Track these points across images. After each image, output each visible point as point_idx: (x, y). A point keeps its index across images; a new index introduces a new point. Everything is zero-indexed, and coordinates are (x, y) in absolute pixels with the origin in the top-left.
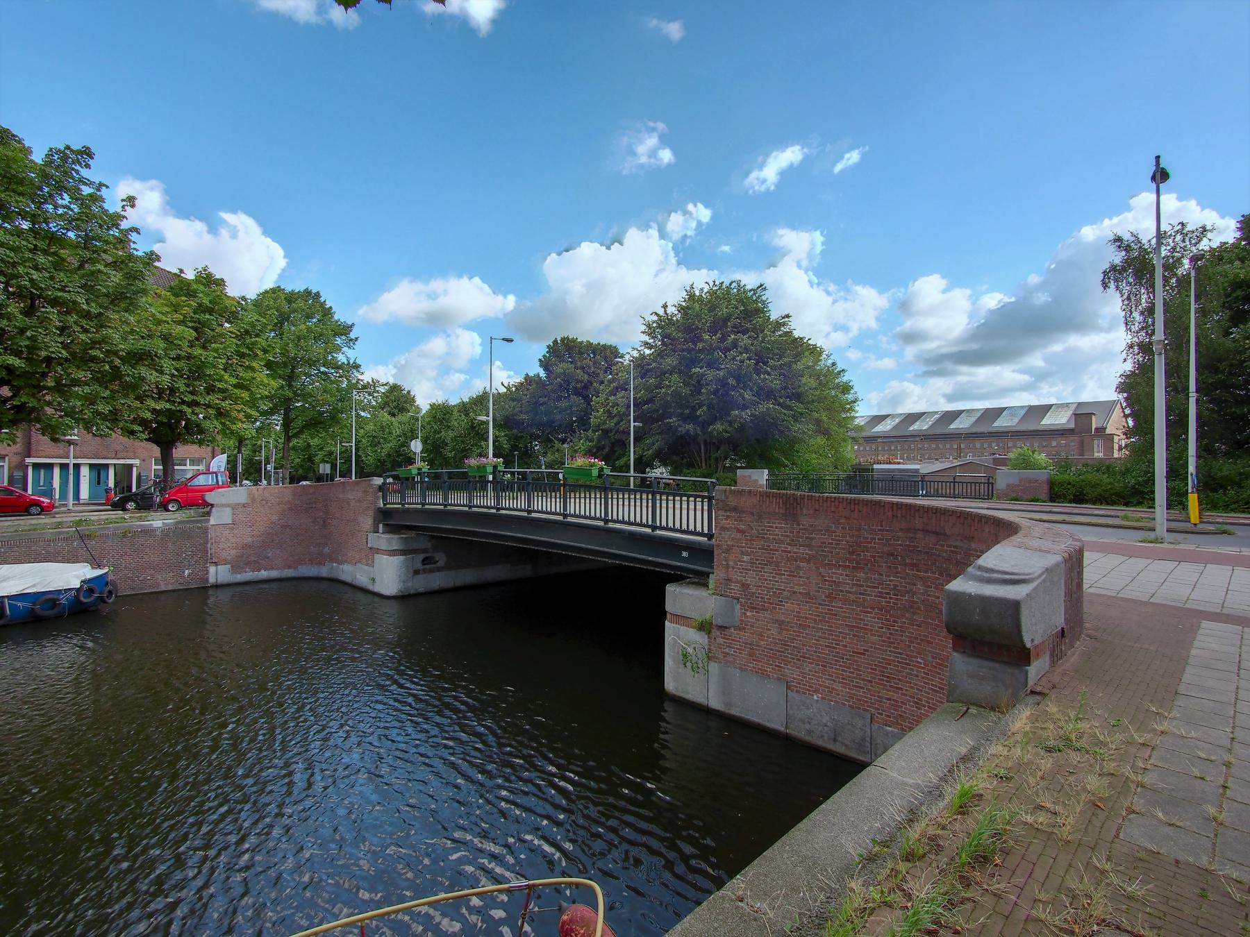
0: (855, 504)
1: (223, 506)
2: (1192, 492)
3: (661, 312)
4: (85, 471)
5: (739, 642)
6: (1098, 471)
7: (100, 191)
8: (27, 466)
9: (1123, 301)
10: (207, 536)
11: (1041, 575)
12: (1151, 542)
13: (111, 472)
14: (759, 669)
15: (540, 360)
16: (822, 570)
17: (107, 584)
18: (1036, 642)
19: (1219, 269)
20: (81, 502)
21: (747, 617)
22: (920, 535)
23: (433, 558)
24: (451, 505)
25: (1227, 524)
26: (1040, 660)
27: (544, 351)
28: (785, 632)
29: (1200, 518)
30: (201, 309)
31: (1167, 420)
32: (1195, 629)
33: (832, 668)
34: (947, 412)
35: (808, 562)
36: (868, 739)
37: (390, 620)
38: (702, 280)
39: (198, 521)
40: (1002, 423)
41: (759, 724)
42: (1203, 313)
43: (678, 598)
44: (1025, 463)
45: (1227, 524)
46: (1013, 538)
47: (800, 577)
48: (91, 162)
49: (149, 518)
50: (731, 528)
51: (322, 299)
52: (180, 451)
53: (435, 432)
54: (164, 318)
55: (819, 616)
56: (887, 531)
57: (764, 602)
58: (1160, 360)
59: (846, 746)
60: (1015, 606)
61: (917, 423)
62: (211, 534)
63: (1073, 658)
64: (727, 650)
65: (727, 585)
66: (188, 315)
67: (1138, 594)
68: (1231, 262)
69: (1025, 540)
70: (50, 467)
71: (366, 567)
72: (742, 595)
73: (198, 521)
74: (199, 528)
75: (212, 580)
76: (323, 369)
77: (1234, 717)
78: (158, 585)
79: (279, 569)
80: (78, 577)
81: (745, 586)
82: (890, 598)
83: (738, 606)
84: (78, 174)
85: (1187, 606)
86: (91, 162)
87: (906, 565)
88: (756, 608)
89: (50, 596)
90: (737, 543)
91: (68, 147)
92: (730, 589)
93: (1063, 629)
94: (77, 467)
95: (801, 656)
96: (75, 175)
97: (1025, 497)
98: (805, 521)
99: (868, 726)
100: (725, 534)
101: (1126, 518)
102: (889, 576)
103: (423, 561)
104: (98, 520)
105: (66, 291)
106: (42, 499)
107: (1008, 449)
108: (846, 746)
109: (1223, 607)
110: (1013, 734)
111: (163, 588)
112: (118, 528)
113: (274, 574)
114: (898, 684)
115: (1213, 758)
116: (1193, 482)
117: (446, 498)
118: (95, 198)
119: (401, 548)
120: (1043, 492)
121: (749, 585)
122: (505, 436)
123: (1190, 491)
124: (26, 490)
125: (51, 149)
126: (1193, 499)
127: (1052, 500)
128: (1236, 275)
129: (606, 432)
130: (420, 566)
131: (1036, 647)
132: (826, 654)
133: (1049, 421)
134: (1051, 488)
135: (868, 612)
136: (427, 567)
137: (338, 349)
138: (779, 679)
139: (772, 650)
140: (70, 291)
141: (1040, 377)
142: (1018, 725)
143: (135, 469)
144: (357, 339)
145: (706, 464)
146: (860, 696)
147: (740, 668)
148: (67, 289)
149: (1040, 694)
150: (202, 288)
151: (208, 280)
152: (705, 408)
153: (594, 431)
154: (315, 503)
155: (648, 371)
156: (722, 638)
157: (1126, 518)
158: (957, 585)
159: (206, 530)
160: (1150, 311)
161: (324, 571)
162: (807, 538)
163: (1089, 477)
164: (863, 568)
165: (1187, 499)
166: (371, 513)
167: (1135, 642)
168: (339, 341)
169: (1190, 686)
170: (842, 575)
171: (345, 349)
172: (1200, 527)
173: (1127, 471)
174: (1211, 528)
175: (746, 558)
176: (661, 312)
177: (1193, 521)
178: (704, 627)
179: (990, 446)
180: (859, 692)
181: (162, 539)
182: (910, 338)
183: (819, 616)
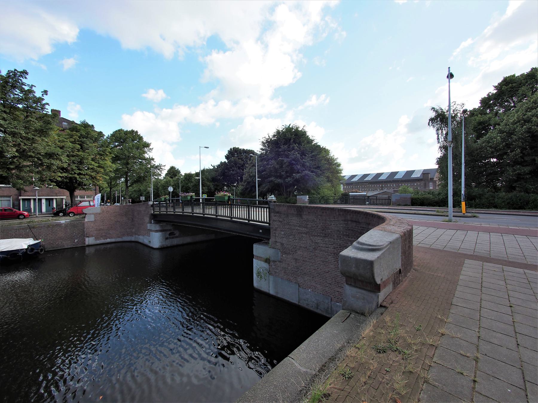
0: (324, 210)
1: (90, 214)
2: (463, 201)
4: (44, 201)
5: (280, 267)
6: (429, 194)
7: (32, 88)
8: (20, 200)
10: (84, 226)
11: (387, 246)
12: (447, 221)
13: (55, 201)
14: (288, 278)
15: (225, 156)
16: (311, 237)
17: (40, 247)
18: (384, 280)
19: (473, 118)
21: (283, 257)
22: (349, 222)
23: (173, 233)
24: (186, 213)
25: (475, 213)
26: (386, 288)
28: (297, 263)
29: (466, 211)
30: (81, 136)
31: (453, 174)
32: (462, 264)
33: (316, 278)
35: (306, 234)
36: (330, 308)
37: (157, 258)
39: (80, 220)
41: (288, 301)
42: (467, 134)
43: (258, 249)
44: (405, 191)
45: (475, 213)
46: (381, 226)
47: (303, 240)
48: (27, 76)
49: (60, 219)
51: (139, 134)
52: (77, 192)
53: (186, 184)
54: (66, 140)
55: (310, 257)
56: (337, 221)
57: (290, 251)
58: (450, 150)
59: (322, 311)
60: (371, 263)
62: (86, 225)
63: (405, 284)
64: (276, 271)
65: (275, 244)
66: (76, 139)
67: (439, 246)
68: (477, 115)
69: (386, 226)
71: (147, 237)
73: (80, 220)
74: (80, 223)
75: (87, 243)
76: (140, 160)
77: (480, 320)
79: (114, 238)
80: (26, 244)
81: (282, 244)
82: (338, 249)
83: (280, 253)
84: (21, 81)
85: (459, 252)
86: (27, 76)
87: (344, 235)
89: (14, 252)
91: (15, 70)
92: (277, 245)
93: (400, 269)
94: (40, 200)
95: (304, 273)
96: (20, 81)
97: (402, 204)
98: (305, 217)
99: (330, 303)
101: (438, 212)
102: (338, 240)
103: (169, 234)
104: (38, 221)
105: (16, 129)
106: (24, 213)
107: (399, 187)
108: (322, 311)
109: (474, 252)
110: (363, 338)
111: (66, 247)
112: (46, 224)
113: (113, 240)
114: (341, 285)
115: (468, 355)
116: (463, 197)
117: (193, 210)
118: (30, 91)
119: (160, 229)
120: (409, 202)
121: (284, 244)
122: (213, 184)
123: (462, 201)
124: (20, 209)
125: (9, 71)
126: (463, 204)
127: (412, 205)
128: (480, 120)
129: (249, 183)
130: (168, 236)
131: (384, 282)
132: (313, 272)
134: (412, 201)
135: (329, 255)
136: (171, 236)
137: (145, 152)
138: (296, 283)
139: (293, 271)
140: (18, 129)
142: (367, 331)
143: (64, 200)
146: (327, 290)
147: (281, 278)
148: (17, 128)
149: (385, 307)
150: (83, 128)
151: (120, 131)
153: (244, 182)
154: (129, 212)
155: (264, 159)
157: (438, 212)
158: (349, 252)
159: (84, 224)
160: (447, 134)
161: (133, 239)
163: (425, 196)
164: (327, 237)
165: (461, 204)
166: (149, 216)
167: (435, 273)
168: (146, 149)
169: (459, 299)
171: (148, 153)
172: (466, 214)
173: (439, 194)
174: (469, 215)
175: (282, 233)
178: (267, 261)
179: (393, 185)
180: (326, 288)
181: (65, 227)
183: (310, 257)
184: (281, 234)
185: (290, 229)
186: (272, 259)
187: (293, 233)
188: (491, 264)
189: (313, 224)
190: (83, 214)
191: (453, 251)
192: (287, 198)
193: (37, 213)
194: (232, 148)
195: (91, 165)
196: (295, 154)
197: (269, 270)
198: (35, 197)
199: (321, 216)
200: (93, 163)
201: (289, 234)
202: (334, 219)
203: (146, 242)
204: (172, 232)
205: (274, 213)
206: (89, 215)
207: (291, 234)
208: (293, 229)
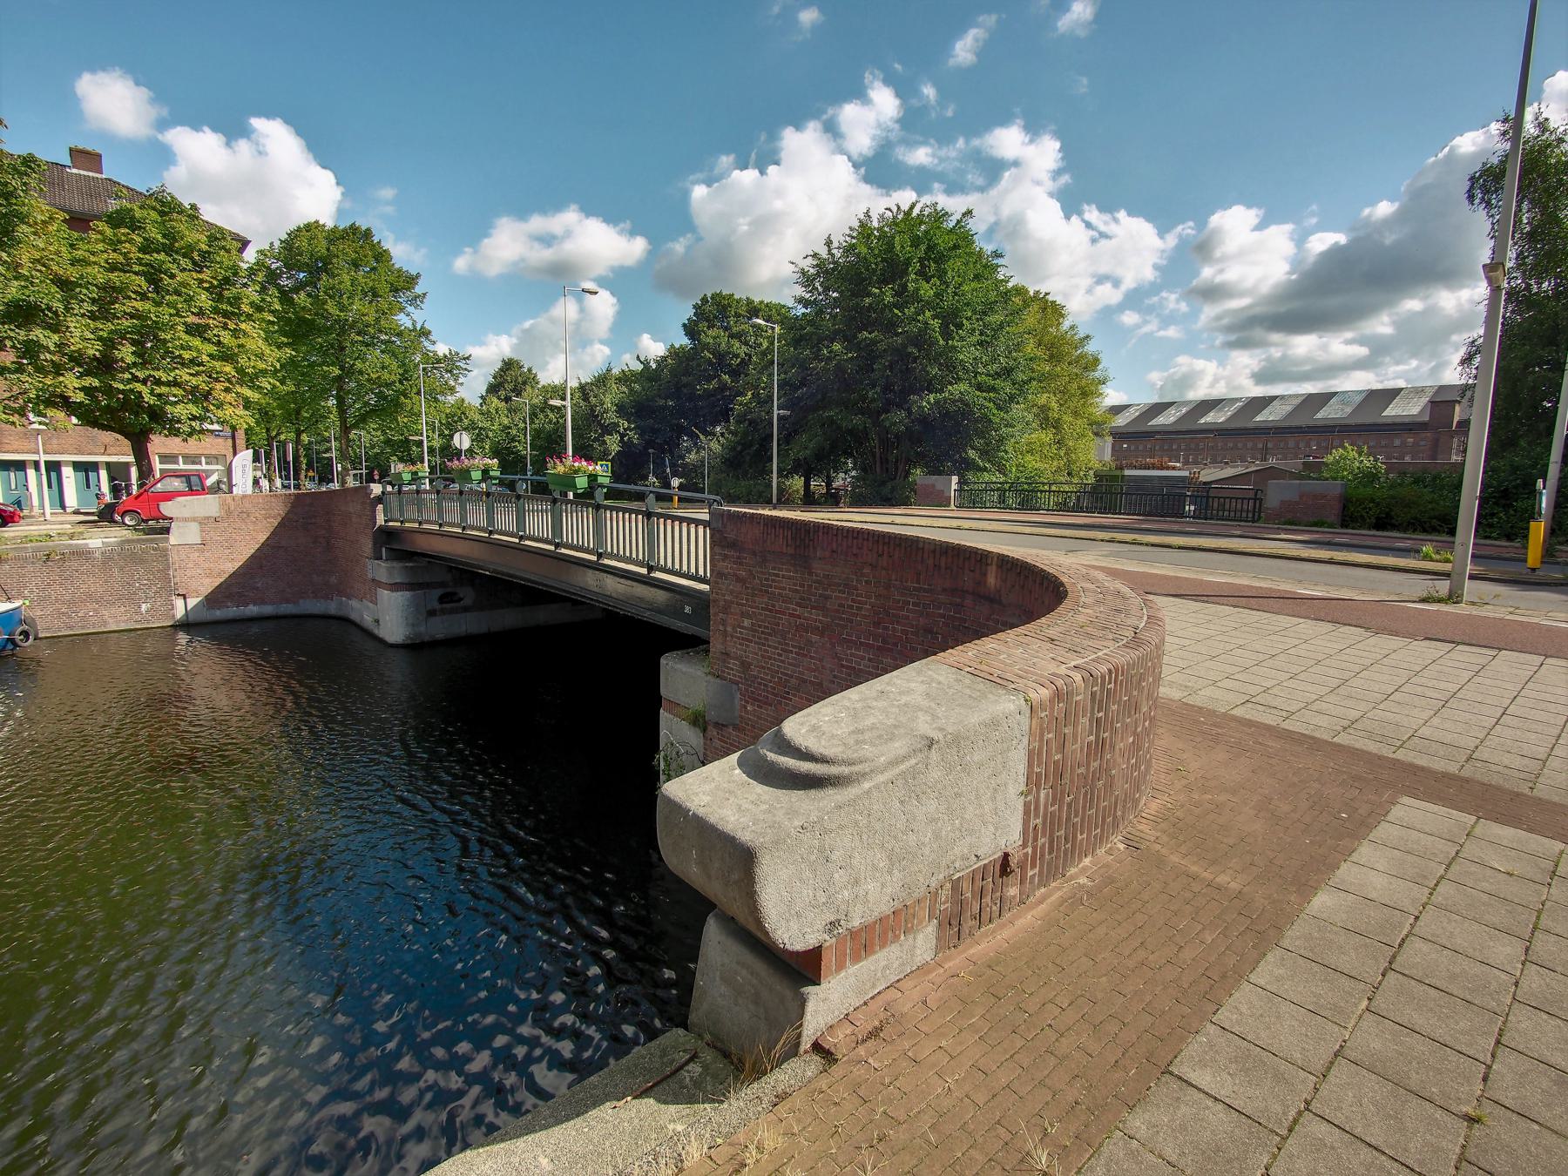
1: (186, 520)
3: (824, 253)
9: (1493, 224)
10: (167, 560)
15: (684, 325)
16: (839, 648)
20: (68, 510)
21: (747, 712)
22: (968, 601)
23: (455, 594)
27: (690, 312)
34: (1254, 398)
35: (822, 635)
38: (880, 205)
40: (1328, 413)
47: (811, 658)
50: (729, 573)
54: (92, 259)
61: (1212, 414)
62: (174, 557)
65: (724, 661)
70: (94, 466)
72: (741, 678)
78: (105, 623)
88: (759, 701)
90: (737, 597)
93: (1006, 855)
94: (53, 467)
100: (723, 584)
104: (14, 538)
107: (1328, 451)
113: (268, 610)
119: (407, 581)
120: (1333, 515)
121: (751, 664)
127: (1344, 525)
130: (437, 606)
133: (1393, 411)
136: (444, 606)
141: (1380, 350)
144: (425, 294)
145: (882, 468)
152: (878, 389)
156: (719, 739)
161: (332, 608)
162: (821, 595)
170: (863, 658)
171: (410, 309)
175: (746, 623)
176: (824, 253)
177: (1530, 563)
181: (104, 563)
182: (1212, 293)
184: (743, 628)
185: (770, 611)
186: (712, 715)
187: (778, 624)
188: (1512, 830)
189: (846, 599)
190: (165, 518)
191: (1372, 747)
192: (883, 483)
193: (48, 511)
194: (709, 295)
195: (190, 348)
196: (920, 318)
197: (704, 754)
198: (35, 457)
199: (874, 567)
200: (196, 342)
201: (766, 627)
202: (918, 582)
203: (367, 620)
204: (449, 590)
205: (723, 547)
206: (181, 524)
207: (773, 630)
208: (780, 612)
